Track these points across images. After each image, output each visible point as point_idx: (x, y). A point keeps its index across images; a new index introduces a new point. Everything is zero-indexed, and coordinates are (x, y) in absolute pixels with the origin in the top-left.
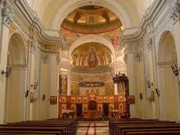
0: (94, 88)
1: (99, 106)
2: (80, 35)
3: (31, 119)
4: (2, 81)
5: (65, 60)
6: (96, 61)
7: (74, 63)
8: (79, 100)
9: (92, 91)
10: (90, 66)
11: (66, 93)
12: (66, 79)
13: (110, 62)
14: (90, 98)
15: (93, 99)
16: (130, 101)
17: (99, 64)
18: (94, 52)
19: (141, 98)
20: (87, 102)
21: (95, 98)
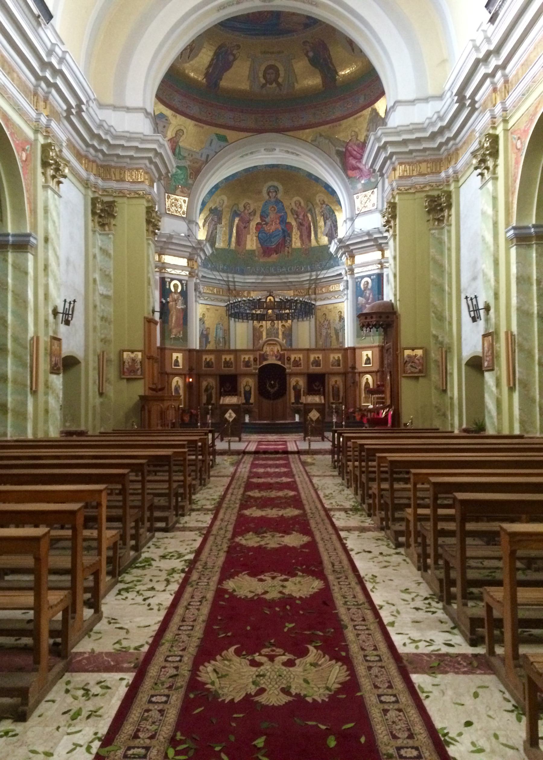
0: (279, 324)
1: (293, 381)
2: (231, 135)
3: (30, 436)
4: (408, 563)
5: (181, 228)
6: (286, 234)
7: (211, 239)
8: (227, 364)
9: (272, 333)
10: (267, 251)
11: (185, 338)
12: (184, 294)
13: (332, 234)
14: (264, 357)
15: (272, 360)
16: (147, 643)
17: (296, 243)
18: (278, 202)
19: (39, 716)
20: (254, 369)
21: (281, 357)
